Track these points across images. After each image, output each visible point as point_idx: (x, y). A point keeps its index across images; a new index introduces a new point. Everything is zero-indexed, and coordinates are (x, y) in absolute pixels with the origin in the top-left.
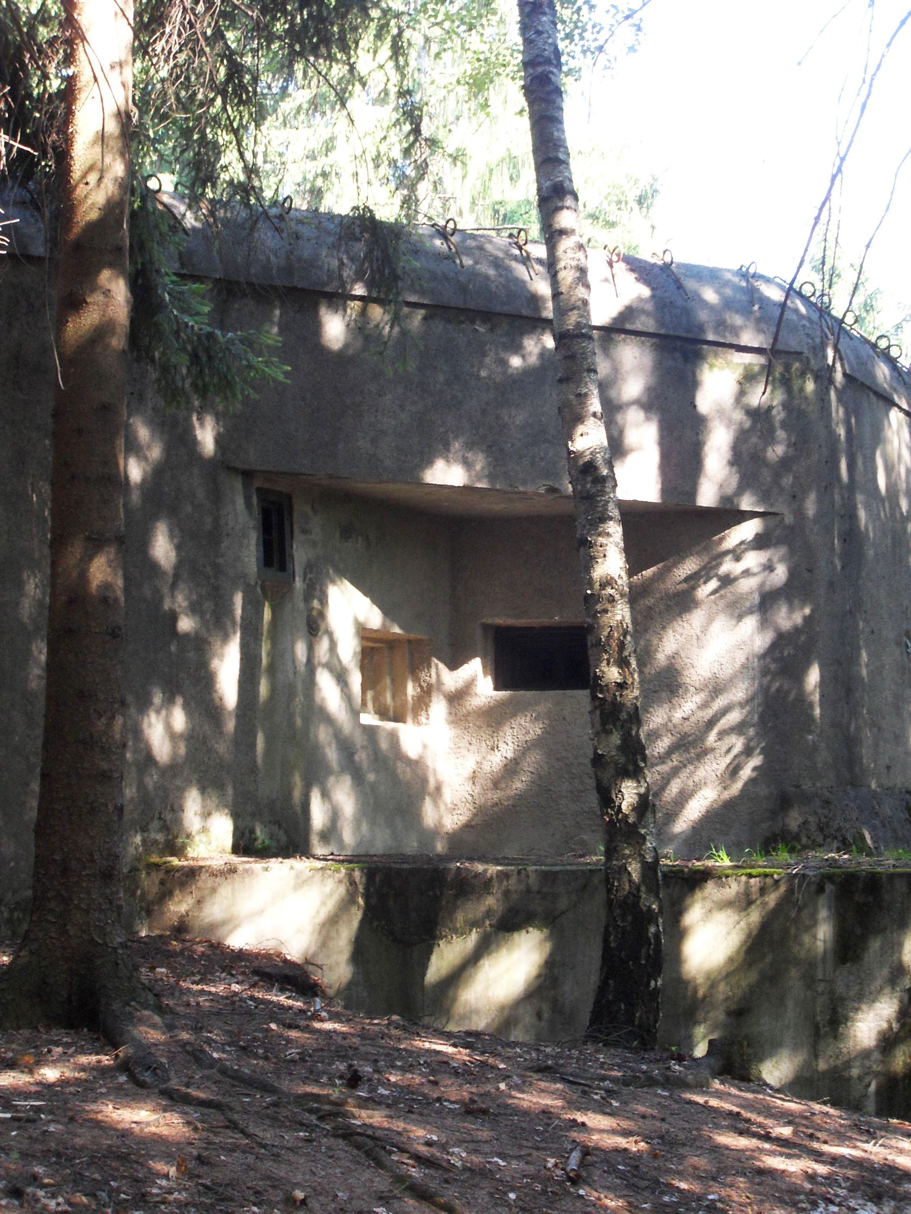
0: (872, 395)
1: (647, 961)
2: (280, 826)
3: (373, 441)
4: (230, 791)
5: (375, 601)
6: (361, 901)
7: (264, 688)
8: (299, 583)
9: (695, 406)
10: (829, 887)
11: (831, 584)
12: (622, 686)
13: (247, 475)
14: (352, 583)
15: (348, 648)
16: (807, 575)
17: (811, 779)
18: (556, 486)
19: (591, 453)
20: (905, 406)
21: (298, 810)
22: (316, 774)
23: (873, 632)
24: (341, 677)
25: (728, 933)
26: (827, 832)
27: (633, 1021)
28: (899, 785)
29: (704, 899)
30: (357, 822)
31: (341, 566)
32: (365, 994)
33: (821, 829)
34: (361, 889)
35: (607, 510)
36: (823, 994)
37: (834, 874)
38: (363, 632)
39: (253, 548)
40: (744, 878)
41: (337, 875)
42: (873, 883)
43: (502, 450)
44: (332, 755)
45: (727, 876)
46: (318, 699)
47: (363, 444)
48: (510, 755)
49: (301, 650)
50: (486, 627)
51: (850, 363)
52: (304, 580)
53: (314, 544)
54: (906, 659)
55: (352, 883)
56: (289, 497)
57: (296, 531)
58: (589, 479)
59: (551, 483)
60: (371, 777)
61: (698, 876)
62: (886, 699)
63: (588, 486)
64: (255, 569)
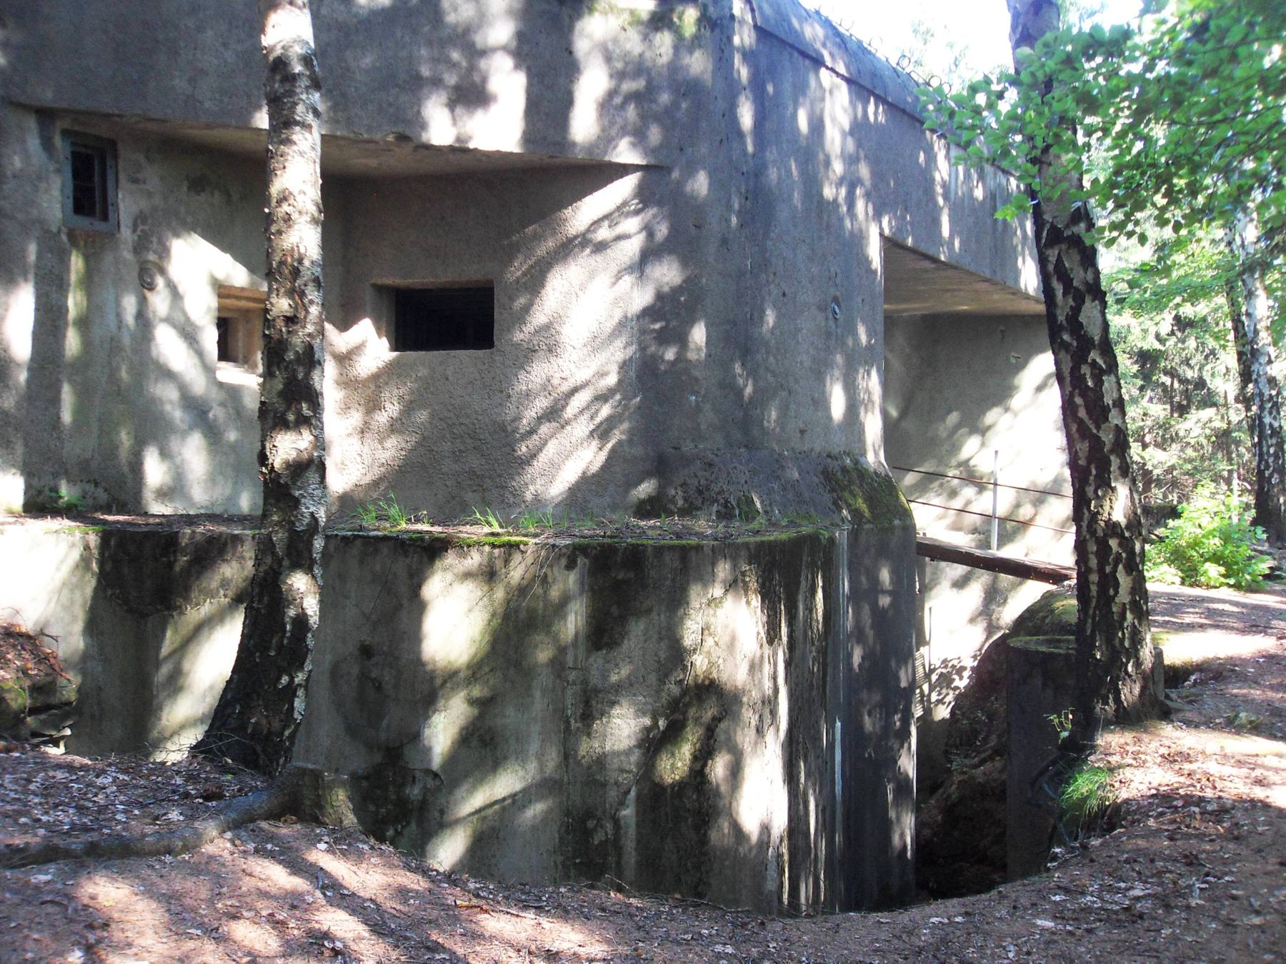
0: (796, 54)
1: (278, 653)
2: (96, 484)
3: (192, 81)
4: (20, 449)
5: (237, 257)
6: (95, 566)
7: (72, 342)
8: (126, 234)
9: (571, 53)
10: (581, 561)
11: (724, 241)
12: (291, 320)
13: (45, 115)
14: (204, 237)
15: (202, 308)
16: (693, 231)
17: (693, 440)
18: (408, 133)
19: (283, 48)
20: (842, 69)
21: (126, 469)
22: (152, 429)
23: (784, 294)
24: (189, 334)
25: (470, 611)
26: (707, 494)
27: (246, 729)
28: (818, 449)
29: (445, 570)
30: (212, 480)
31: (189, 219)
32: (100, 669)
33: (700, 492)
34: (95, 552)
35: (294, 113)
36: (574, 683)
37: (588, 546)
38: (222, 290)
39: (56, 193)
40: (487, 548)
41: (71, 538)
42: (635, 557)
43: (344, 95)
44: (177, 415)
45: (469, 546)
46: (154, 353)
47: (180, 84)
48: (395, 415)
49: (129, 304)
50: (380, 289)
51: (762, 14)
52: (134, 231)
53: (149, 195)
54: (831, 323)
55: (87, 547)
56: (113, 143)
57: (122, 177)
58: (278, 77)
59: (400, 130)
60: (232, 436)
61: (438, 545)
62: (801, 363)
63: (277, 86)
64: (59, 215)
